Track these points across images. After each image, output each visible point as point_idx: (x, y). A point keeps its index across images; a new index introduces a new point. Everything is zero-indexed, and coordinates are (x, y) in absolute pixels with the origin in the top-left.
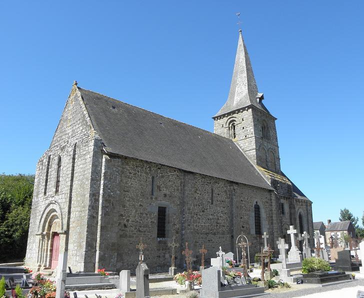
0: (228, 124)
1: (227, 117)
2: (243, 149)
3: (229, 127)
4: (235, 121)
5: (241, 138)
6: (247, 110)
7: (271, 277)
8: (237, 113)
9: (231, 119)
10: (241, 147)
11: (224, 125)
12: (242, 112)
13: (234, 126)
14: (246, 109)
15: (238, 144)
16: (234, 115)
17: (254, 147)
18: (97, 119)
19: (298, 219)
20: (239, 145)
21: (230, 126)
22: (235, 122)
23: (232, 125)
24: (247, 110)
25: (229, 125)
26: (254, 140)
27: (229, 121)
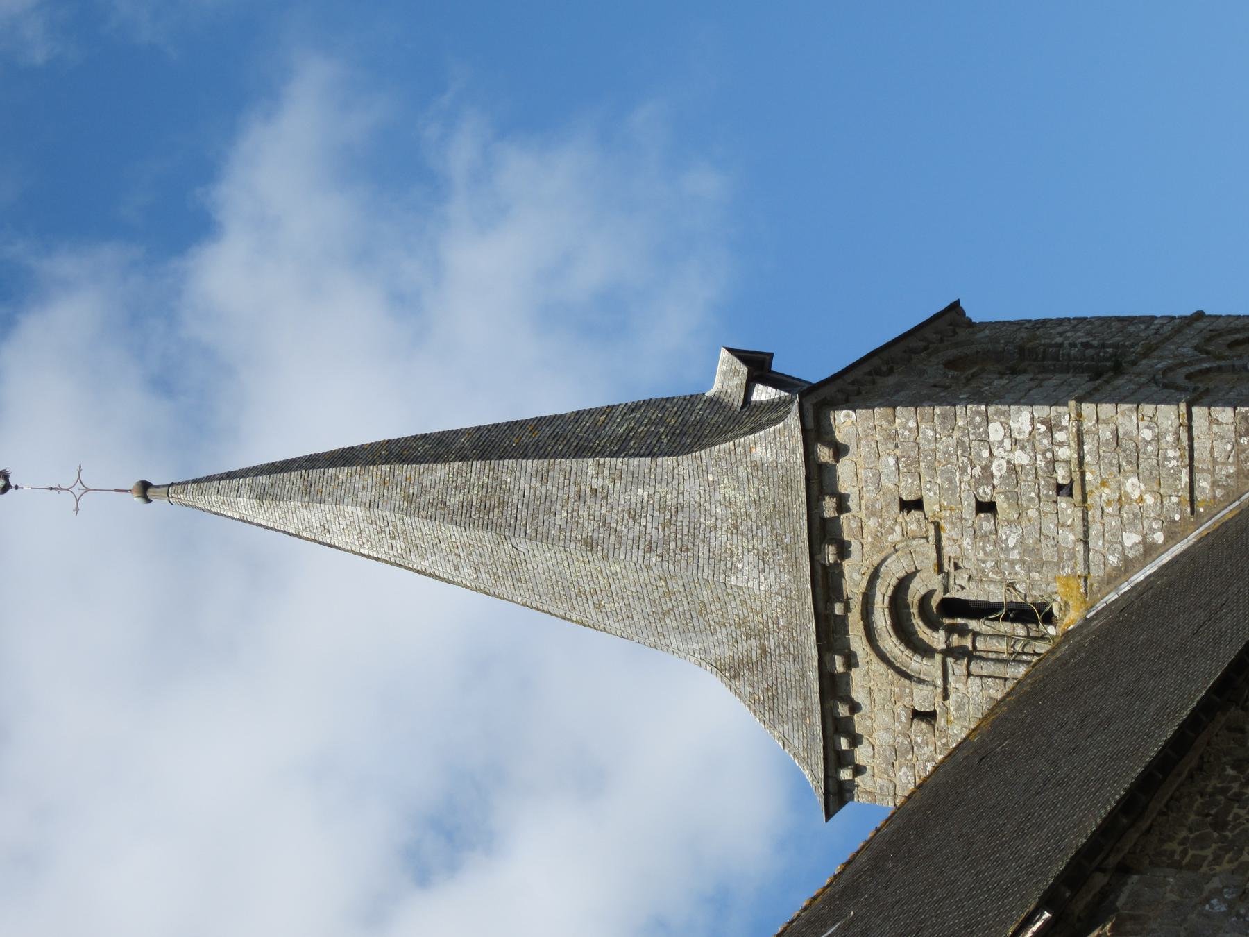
0: (916, 663)
1: (851, 661)
2: (1172, 536)
3: (949, 652)
4: (903, 585)
5: (1070, 538)
6: (840, 451)
7: (944, 594)
8: (844, 550)
9: (882, 618)
10: (1150, 550)
11: (923, 698)
12: (842, 506)
13: (954, 607)
14: (824, 454)
15: (1111, 579)
16: (854, 580)
17: (1168, 415)
18: (1146, 590)
19: (1214, 519)
20: (1128, 565)
21: (937, 640)
22: (917, 590)
23: (933, 625)
24: (840, 451)
25: (925, 651)
26: (1106, 409)
27: (891, 644)
